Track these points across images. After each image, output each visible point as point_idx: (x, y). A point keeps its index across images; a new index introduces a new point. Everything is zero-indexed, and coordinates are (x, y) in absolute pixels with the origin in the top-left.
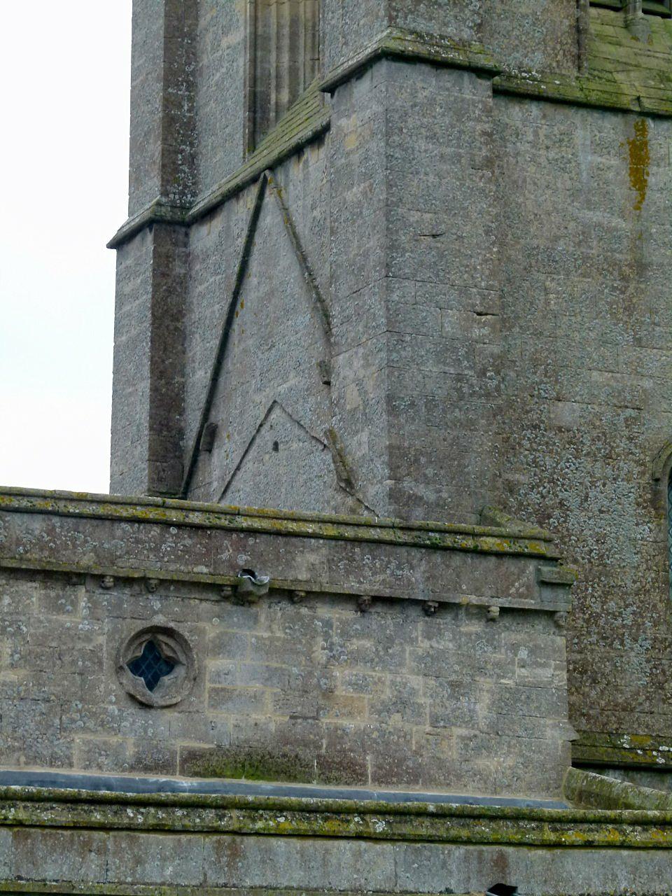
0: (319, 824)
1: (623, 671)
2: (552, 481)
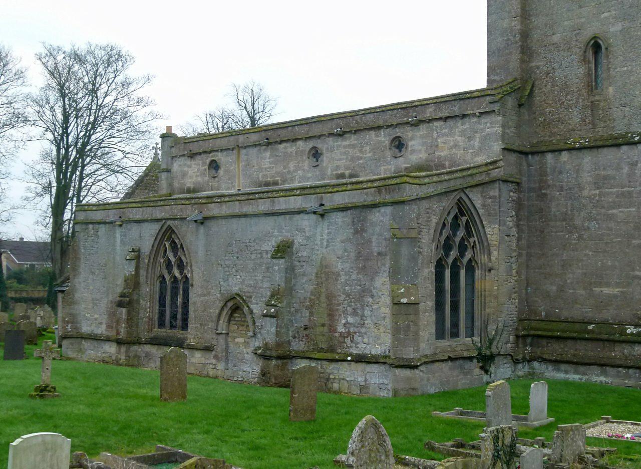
0: (288, 194)
1: (572, 118)
2: (551, 62)
